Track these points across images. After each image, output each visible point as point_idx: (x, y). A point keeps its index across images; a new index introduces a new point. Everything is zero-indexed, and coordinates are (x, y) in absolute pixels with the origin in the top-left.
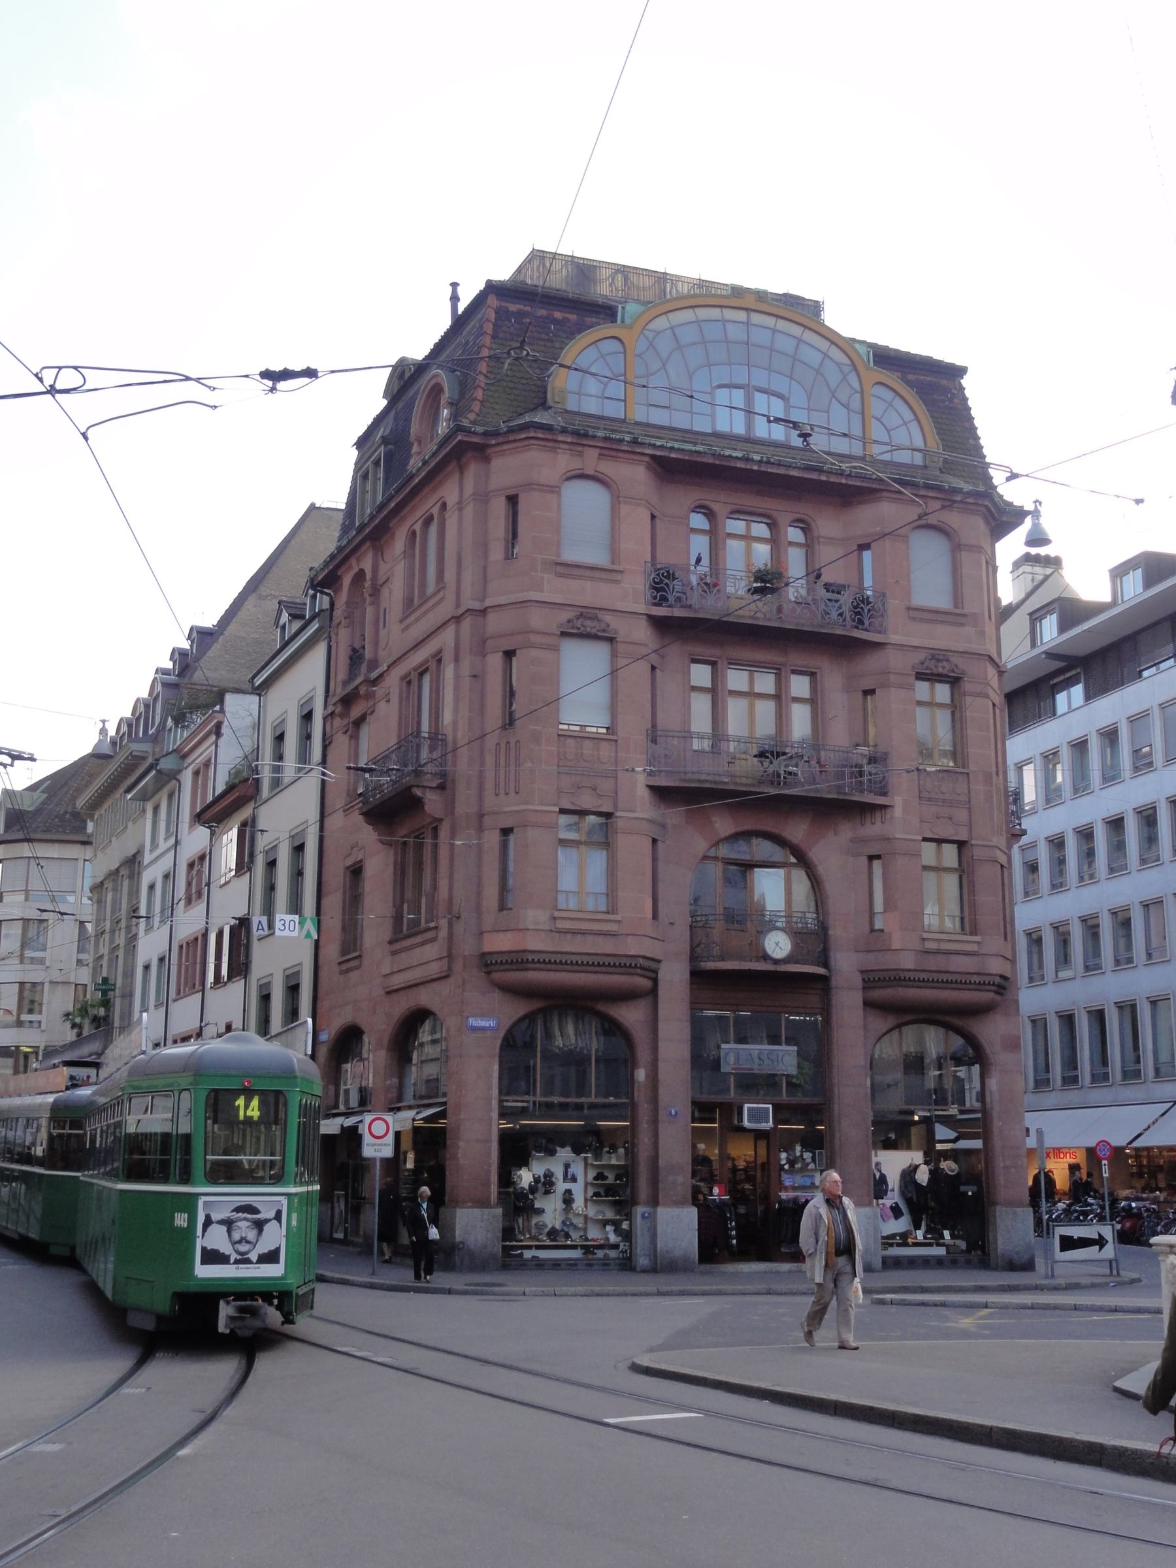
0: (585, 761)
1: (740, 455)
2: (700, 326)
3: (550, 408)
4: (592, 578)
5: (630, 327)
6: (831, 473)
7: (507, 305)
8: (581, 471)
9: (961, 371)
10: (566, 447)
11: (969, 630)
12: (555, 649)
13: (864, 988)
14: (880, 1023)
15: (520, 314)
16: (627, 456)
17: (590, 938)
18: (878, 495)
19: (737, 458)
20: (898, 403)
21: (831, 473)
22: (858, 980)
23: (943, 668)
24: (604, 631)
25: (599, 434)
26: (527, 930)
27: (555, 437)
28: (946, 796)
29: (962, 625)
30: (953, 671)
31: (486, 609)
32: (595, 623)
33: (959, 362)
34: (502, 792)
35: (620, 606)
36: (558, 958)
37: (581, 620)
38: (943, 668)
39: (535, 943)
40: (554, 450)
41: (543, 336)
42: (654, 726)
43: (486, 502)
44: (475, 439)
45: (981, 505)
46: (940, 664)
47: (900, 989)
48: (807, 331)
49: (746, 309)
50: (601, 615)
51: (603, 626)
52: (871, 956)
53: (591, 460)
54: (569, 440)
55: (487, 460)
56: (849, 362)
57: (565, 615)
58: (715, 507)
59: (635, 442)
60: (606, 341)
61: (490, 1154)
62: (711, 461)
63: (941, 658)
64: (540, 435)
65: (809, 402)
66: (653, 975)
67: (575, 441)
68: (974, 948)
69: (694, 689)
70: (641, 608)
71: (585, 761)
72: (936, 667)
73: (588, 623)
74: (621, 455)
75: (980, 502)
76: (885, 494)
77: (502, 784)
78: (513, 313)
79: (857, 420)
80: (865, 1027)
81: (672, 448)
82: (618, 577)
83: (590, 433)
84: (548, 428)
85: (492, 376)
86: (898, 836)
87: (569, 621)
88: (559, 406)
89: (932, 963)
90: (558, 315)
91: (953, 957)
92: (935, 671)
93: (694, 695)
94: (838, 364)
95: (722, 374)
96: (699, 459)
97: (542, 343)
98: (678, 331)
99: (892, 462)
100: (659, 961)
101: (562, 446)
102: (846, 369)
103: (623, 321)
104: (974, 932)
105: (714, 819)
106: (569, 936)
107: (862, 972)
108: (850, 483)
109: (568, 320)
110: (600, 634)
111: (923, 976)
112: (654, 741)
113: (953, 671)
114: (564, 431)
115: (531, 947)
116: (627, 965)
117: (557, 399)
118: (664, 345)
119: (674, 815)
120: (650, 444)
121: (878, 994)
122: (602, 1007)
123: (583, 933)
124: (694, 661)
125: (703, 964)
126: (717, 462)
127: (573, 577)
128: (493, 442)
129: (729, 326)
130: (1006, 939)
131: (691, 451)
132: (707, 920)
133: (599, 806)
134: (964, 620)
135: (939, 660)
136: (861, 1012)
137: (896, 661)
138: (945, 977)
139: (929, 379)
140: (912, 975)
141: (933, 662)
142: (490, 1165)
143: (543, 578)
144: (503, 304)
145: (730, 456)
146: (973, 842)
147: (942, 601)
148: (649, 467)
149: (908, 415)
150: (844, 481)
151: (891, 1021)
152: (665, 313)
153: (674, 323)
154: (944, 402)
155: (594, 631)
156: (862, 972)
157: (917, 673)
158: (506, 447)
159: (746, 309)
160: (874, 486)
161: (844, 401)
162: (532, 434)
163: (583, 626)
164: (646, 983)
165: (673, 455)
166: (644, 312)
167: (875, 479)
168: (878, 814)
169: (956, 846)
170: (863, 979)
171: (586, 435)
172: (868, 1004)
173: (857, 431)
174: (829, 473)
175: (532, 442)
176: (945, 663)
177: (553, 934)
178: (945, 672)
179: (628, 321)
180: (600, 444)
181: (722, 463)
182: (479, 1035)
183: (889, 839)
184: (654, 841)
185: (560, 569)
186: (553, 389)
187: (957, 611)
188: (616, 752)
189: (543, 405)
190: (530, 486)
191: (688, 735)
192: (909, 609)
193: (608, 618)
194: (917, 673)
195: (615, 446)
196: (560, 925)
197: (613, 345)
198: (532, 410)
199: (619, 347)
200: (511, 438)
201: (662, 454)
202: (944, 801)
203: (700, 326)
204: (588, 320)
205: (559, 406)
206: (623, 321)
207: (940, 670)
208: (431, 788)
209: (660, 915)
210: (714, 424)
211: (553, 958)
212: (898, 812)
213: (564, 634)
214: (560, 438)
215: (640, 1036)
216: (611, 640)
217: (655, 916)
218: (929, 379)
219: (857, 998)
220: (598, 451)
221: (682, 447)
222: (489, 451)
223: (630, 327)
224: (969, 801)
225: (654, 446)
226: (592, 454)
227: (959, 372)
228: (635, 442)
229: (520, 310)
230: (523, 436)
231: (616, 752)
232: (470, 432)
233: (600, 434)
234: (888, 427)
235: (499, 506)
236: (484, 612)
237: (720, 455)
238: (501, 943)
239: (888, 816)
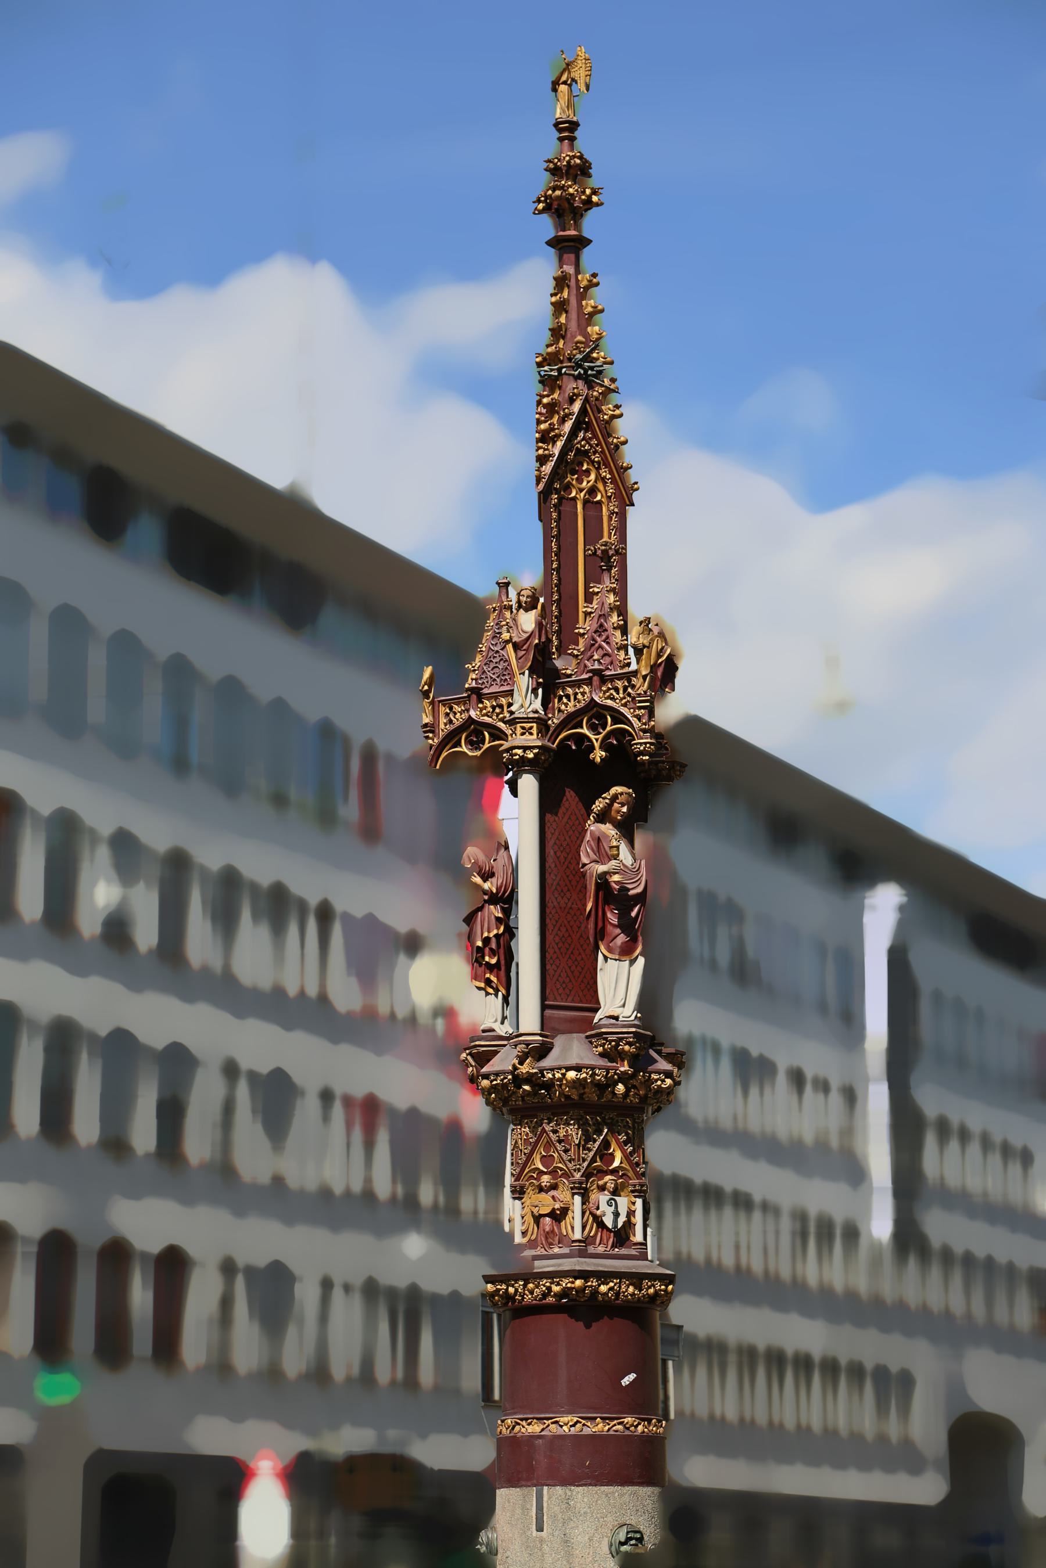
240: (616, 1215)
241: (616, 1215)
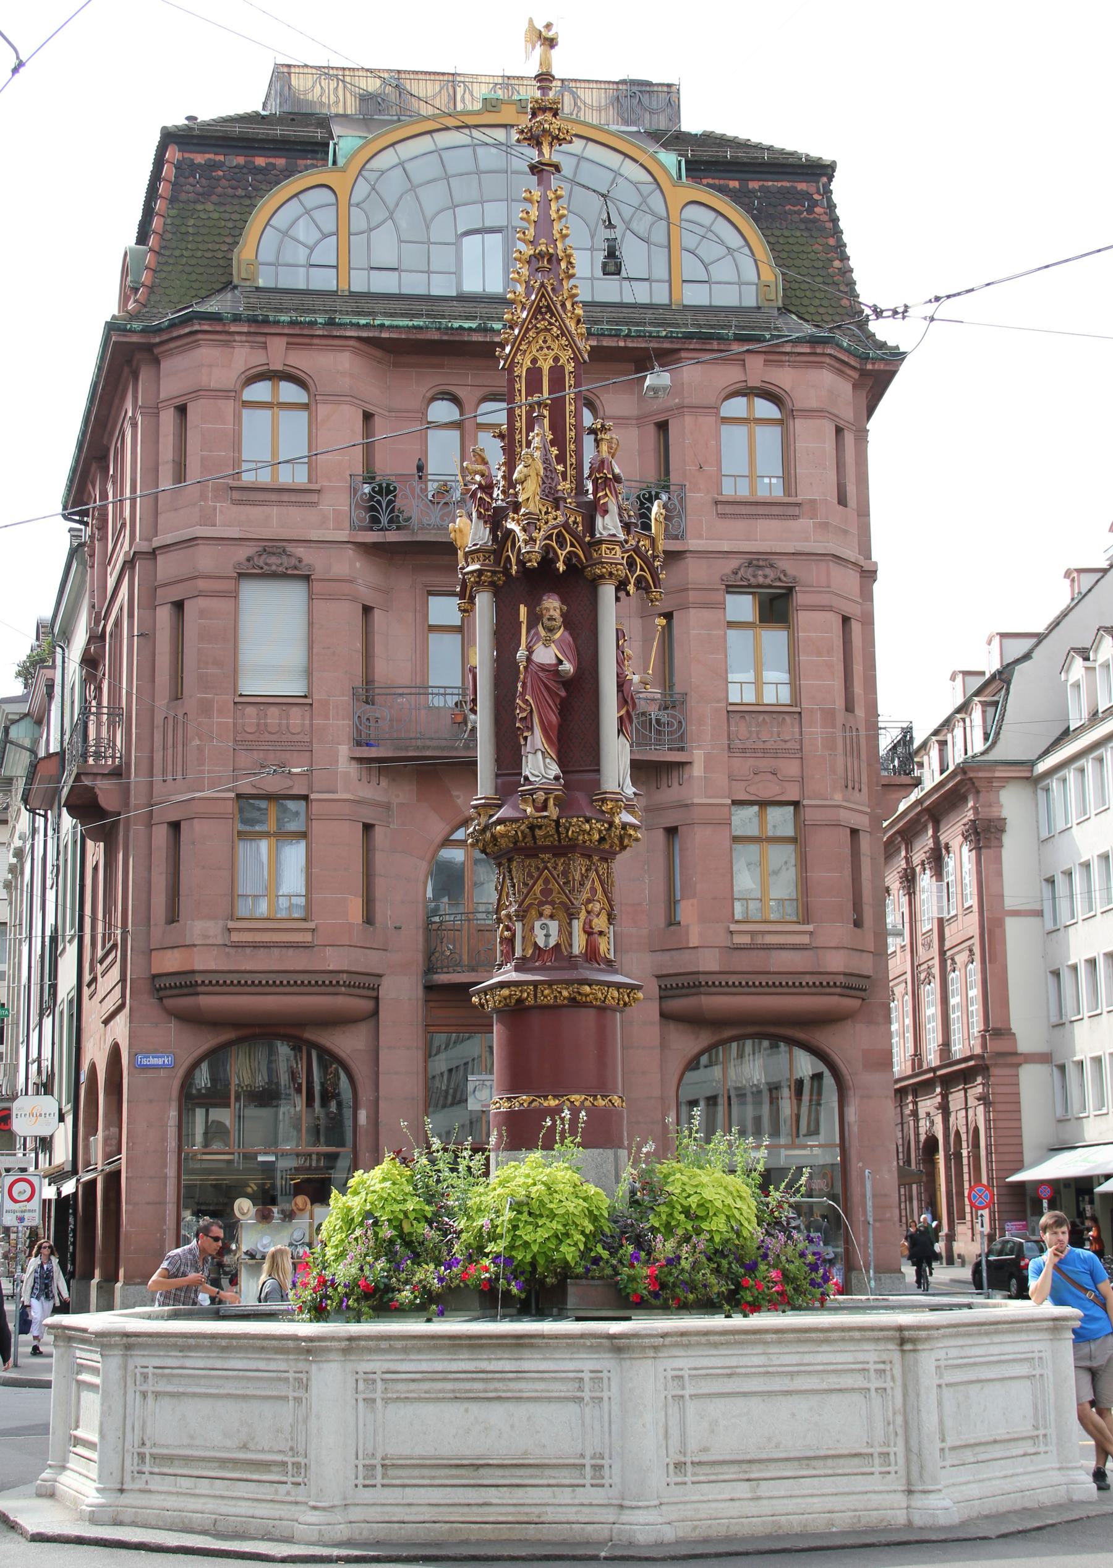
0: (270, 733)
1: (473, 325)
2: (440, 156)
3: (236, 287)
4: (280, 503)
5: (343, 170)
6: (603, 335)
7: (192, 156)
8: (266, 367)
9: (821, 171)
10: (244, 338)
11: (805, 523)
12: (235, 596)
13: (661, 998)
14: (686, 1043)
15: (213, 166)
16: (324, 342)
17: (276, 952)
18: (677, 356)
19: (470, 329)
20: (722, 226)
21: (603, 335)
22: (653, 988)
23: (765, 576)
24: (296, 568)
25: (282, 319)
26: (195, 945)
27: (227, 328)
28: (768, 746)
29: (795, 517)
30: (780, 580)
31: (154, 550)
32: (285, 559)
33: (827, 157)
34: (180, 777)
35: (314, 535)
36: (235, 978)
37: (263, 557)
38: (765, 576)
39: (204, 962)
40: (227, 344)
41: (240, 192)
42: (368, 681)
43: (157, 415)
44: (135, 339)
45: (823, 354)
46: (760, 572)
47: (703, 998)
48: (590, 144)
49: (505, 126)
50: (290, 548)
51: (293, 561)
52: (667, 956)
53: (278, 354)
54: (245, 329)
55: (157, 362)
56: (650, 179)
57: (243, 553)
58: (461, 392)
59: (331, 323)
60: (311, 191)
61: (164, 1218)
62: (436, 336)
63: (761, 563)
64: (206, 328)
65: (592, 237)
66: (374, 994)
67: (252, 330)
68: (806, 939)
69: (434, 628)
70: (343, 535)
71: (270, 733)
72: (755, 576)
73: (273, 560)
74: (316, 341)
75: (819, 351)
76: (683, 354)
77: (170, 768)
78: (200, 165)
79: (661, 256)
80: (664, 1045)
81: (382, 326)
82: (314, 498)
83: (271, 319)
84: (215, 318)
85: (167, 253)
86: (696, 801)
87: (248, 560)
88: (248, 283)
89: (743, 962)
90: (260, 161)
91: (774, 953)
92: (753, 581)
93: (432, 637)
94: (635, 184)
95: (467, 218)
96: (420, 337)
97: (235, 201)
98: (407, 166)
99: (711, 306)
100: (380, 976)
101: (237, 338)
102: (646, 189)
103: (335, 163)
104: (806, 920)
105: (455, 793)
106: (248, 950)
107: (658, 977)
108: (630, 345)
109: (274, 165)
110: (289, 572)
111: (731, 979)
112: (369, 701)
113: (780, 580)
114: (236, 319)
115: (199, 966)
116: (329, 982)
117: (244, 276)
118: (392, 186)
119: (401, 794)
120: (352, 324)
121: (678, 1004)
122: (309, 1035)
123: (267, 946)
124: (431, 593)
125: (436, 977)
126: (445, 338)
127: (254, 503)
128: (157, 340)
129: (480, 151)
130: (858, 924)
131: (407, 327)
132: (441, 922)
133: (291, 787)
134: (796, 511)
135: (759, 567)
136: (655, 1030)
137: (695, 572)
138: (763, 979)
139: (779, 184)
140: (717, 979)
141: (750, 570)
142: (163, 1233)
143: (215, 508)
144: (187, 155)
145: (461, 328)
146: (805, 802)
147: (771, 486)
148: (356, 352)
149: (735, 241)
150: (622, 344)
151: (705, 1039)
152: (393, 145)
153: (403, 158)
154: (800, 213)
155: (281, 569)
156: (658, 977)
157: (728, 586)
158: (172, 345)
159: (505, 126)
160: (667, 345)
161: (643, 233)
162: (197, 328)
163: (267, 564)
164: (368, 1005)
165: (385, 335)
166: (362, 148)
167: (666, 337)
168: (675, 774)
169: (791, 808)
170: (660, 987)
171: (266, 322)
172: (664, 1015)
173: (661, 272)
174: (598, 335)
175: (200, 336)
176: (768, 571)
177: (227, 949)
178: (768, 581)
179: (341, 162)
180: (286, 331)
181: (452, 338)
182: (150, 1075)
183: (687, 806)
184: (368, 828)
185: (236, 495)
186: (239, 262)
187: (787, 500)
188: (311, 719)
189: (228, 285)
190: (197, 393)
191: (423, 689)
192: (716, 503)
193: (300, 551)
194: (728, 586)
195: (306, 332)
196: (236, 937)
197: (325, 196)
198: (220, 291)
199: (331, 198)
200: (175, 334)
201: (371, 334)
202: (764, 751)
203: (440, 156)
204: (301, 162)
205: (248, 283)
206: (335, 163)
207: (761, 580)
208: (103, 775)
209: (379, 917)
210: (459, 283)
211: (229, 978)
212: (697, 770)
213: (241, 575)
214: (233, 329)
215: (361, 1070)
216: (307, 578)
217: (369, 919)
218: (779, 184)
219: (653, 1010)
220: (285, 340)
221: (395, 323)
222: (156, 351)
223: (343, 170)
224: (801, 749)
225: (358, 326)
226: (277, 345)
227: (821, 171)
228: (331, 323)
229: (210, 159)
230: (187, 330)
231: (311, 719)
232: (125, 330)
233: (285, 318)
234: (707, 261)
235: (168, 417)
236: (153, 554)
237: (447, 328)
238: (170, 962)
239: (686, 776)
240: (547, 936)
241: (547, 936)
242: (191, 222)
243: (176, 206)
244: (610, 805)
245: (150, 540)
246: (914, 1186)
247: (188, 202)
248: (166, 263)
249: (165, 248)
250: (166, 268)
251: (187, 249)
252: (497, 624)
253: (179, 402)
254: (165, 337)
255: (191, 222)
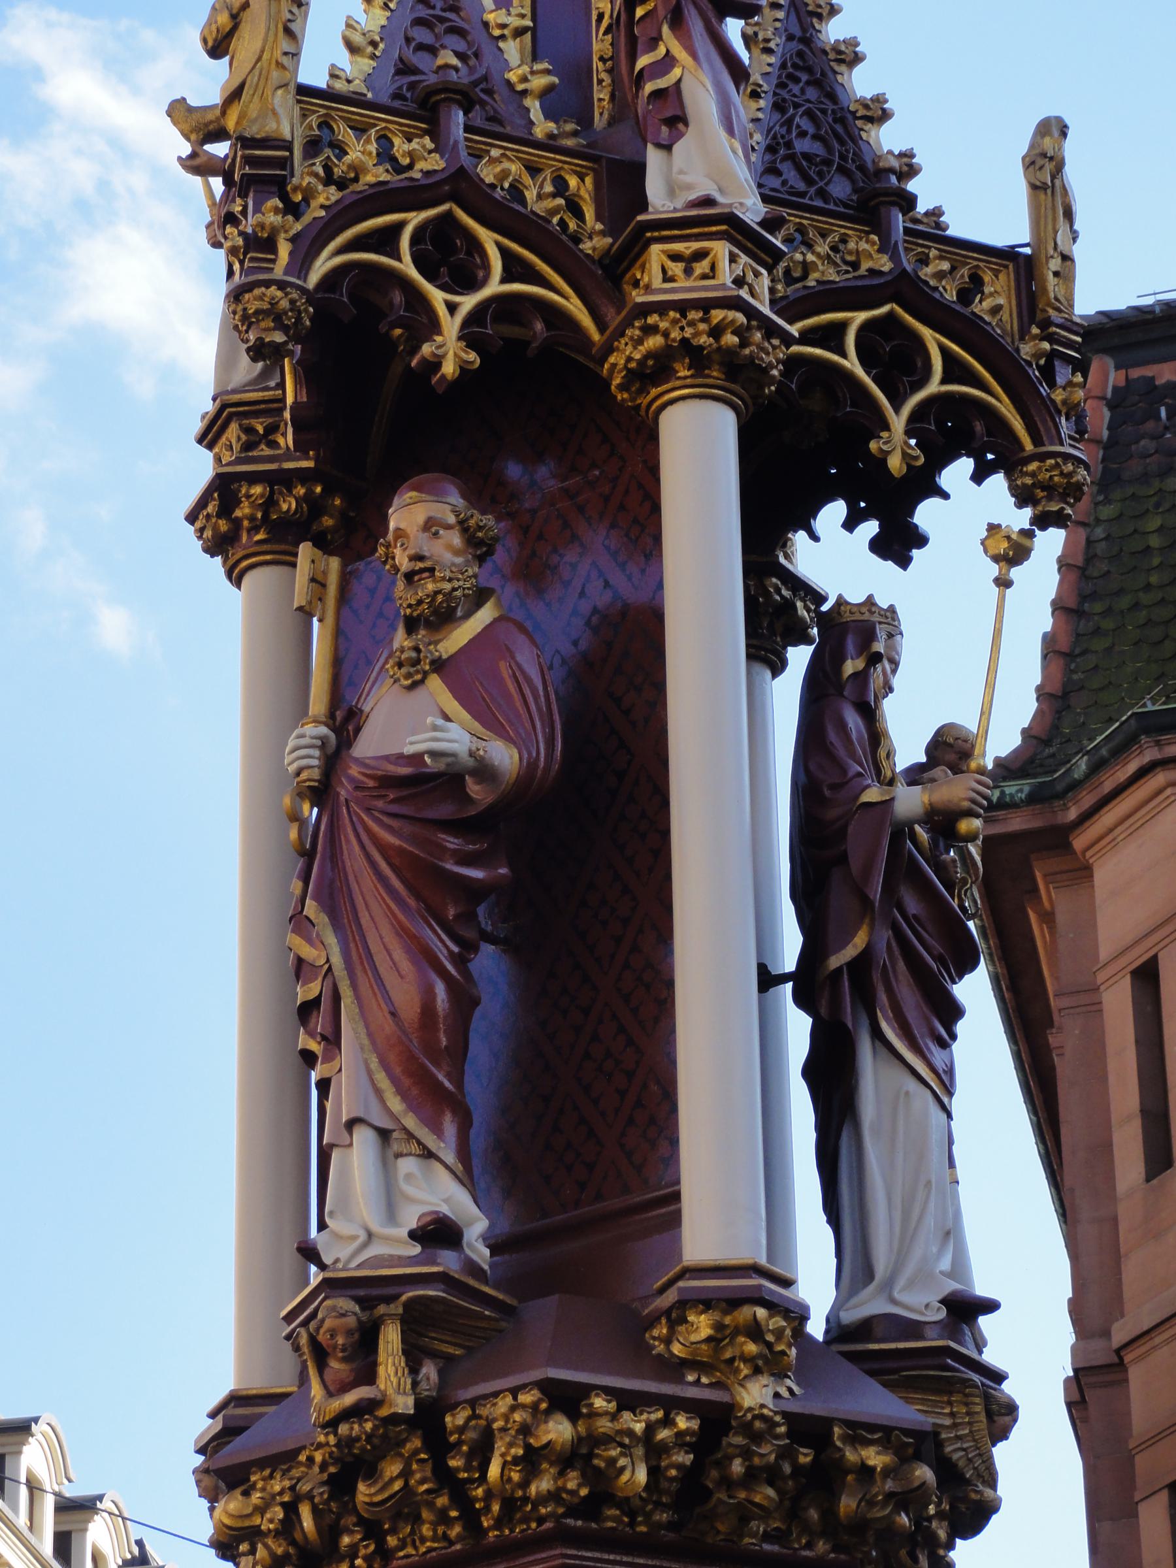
55: (1084, 872)
85: (1098, 607)
144: (1135, 373)
158: (1108, 817)
200: (1108, 786)
222: (1079, 842)
242: (1154, 523)
243: (1117, 494)
244: (702, 1325)
245: (1106, 1334)
246: (1079, 339)
247: (1144, 478)
248: (1097, 632)
249: (1092, 596)
250: (1099, 644)
251: (1148, 587)
252: (1024, 421)
253: (1138, 957)
254: (1087, 800)
255: (1154, 523)
